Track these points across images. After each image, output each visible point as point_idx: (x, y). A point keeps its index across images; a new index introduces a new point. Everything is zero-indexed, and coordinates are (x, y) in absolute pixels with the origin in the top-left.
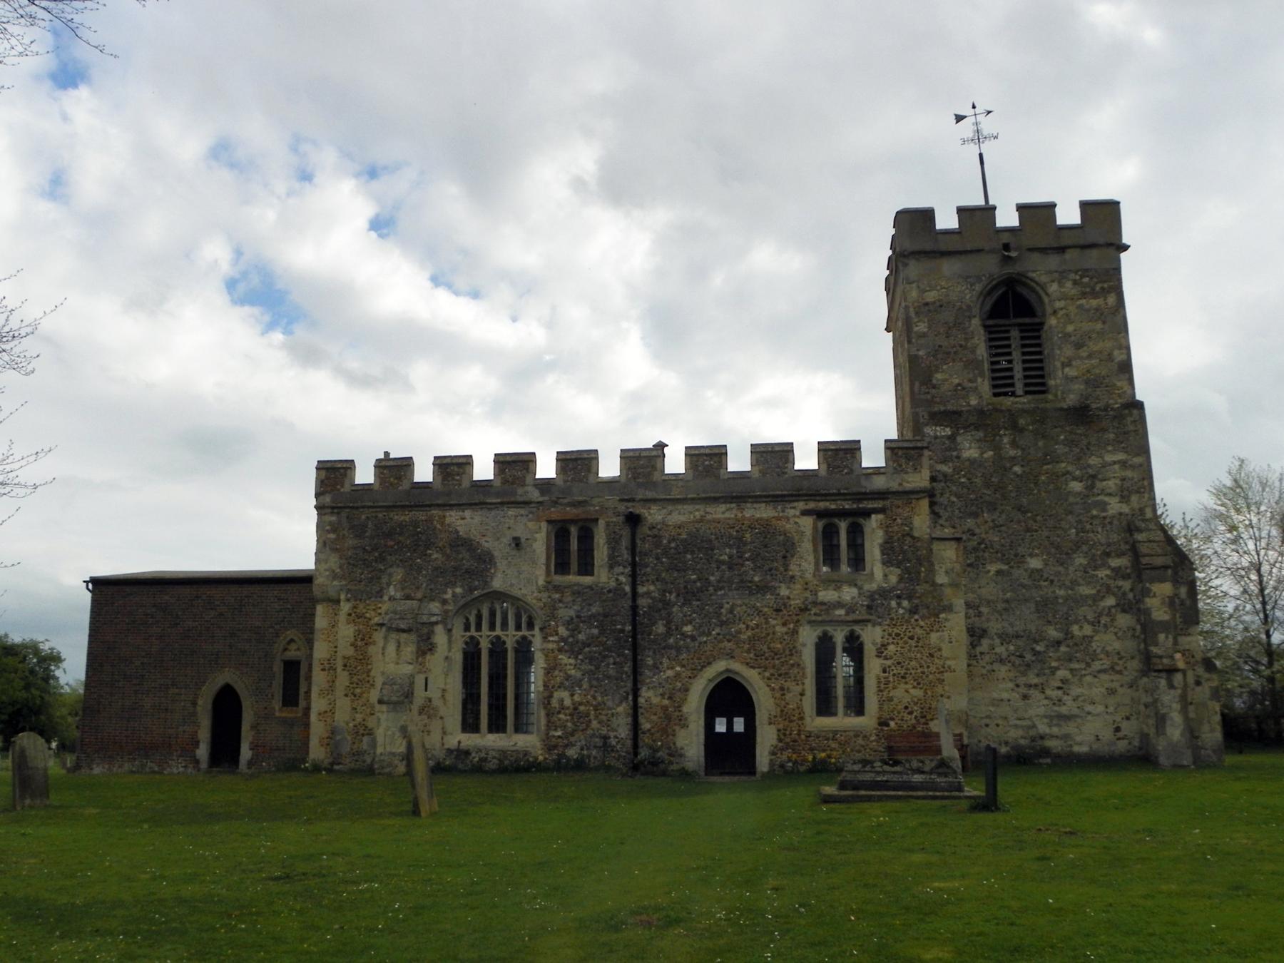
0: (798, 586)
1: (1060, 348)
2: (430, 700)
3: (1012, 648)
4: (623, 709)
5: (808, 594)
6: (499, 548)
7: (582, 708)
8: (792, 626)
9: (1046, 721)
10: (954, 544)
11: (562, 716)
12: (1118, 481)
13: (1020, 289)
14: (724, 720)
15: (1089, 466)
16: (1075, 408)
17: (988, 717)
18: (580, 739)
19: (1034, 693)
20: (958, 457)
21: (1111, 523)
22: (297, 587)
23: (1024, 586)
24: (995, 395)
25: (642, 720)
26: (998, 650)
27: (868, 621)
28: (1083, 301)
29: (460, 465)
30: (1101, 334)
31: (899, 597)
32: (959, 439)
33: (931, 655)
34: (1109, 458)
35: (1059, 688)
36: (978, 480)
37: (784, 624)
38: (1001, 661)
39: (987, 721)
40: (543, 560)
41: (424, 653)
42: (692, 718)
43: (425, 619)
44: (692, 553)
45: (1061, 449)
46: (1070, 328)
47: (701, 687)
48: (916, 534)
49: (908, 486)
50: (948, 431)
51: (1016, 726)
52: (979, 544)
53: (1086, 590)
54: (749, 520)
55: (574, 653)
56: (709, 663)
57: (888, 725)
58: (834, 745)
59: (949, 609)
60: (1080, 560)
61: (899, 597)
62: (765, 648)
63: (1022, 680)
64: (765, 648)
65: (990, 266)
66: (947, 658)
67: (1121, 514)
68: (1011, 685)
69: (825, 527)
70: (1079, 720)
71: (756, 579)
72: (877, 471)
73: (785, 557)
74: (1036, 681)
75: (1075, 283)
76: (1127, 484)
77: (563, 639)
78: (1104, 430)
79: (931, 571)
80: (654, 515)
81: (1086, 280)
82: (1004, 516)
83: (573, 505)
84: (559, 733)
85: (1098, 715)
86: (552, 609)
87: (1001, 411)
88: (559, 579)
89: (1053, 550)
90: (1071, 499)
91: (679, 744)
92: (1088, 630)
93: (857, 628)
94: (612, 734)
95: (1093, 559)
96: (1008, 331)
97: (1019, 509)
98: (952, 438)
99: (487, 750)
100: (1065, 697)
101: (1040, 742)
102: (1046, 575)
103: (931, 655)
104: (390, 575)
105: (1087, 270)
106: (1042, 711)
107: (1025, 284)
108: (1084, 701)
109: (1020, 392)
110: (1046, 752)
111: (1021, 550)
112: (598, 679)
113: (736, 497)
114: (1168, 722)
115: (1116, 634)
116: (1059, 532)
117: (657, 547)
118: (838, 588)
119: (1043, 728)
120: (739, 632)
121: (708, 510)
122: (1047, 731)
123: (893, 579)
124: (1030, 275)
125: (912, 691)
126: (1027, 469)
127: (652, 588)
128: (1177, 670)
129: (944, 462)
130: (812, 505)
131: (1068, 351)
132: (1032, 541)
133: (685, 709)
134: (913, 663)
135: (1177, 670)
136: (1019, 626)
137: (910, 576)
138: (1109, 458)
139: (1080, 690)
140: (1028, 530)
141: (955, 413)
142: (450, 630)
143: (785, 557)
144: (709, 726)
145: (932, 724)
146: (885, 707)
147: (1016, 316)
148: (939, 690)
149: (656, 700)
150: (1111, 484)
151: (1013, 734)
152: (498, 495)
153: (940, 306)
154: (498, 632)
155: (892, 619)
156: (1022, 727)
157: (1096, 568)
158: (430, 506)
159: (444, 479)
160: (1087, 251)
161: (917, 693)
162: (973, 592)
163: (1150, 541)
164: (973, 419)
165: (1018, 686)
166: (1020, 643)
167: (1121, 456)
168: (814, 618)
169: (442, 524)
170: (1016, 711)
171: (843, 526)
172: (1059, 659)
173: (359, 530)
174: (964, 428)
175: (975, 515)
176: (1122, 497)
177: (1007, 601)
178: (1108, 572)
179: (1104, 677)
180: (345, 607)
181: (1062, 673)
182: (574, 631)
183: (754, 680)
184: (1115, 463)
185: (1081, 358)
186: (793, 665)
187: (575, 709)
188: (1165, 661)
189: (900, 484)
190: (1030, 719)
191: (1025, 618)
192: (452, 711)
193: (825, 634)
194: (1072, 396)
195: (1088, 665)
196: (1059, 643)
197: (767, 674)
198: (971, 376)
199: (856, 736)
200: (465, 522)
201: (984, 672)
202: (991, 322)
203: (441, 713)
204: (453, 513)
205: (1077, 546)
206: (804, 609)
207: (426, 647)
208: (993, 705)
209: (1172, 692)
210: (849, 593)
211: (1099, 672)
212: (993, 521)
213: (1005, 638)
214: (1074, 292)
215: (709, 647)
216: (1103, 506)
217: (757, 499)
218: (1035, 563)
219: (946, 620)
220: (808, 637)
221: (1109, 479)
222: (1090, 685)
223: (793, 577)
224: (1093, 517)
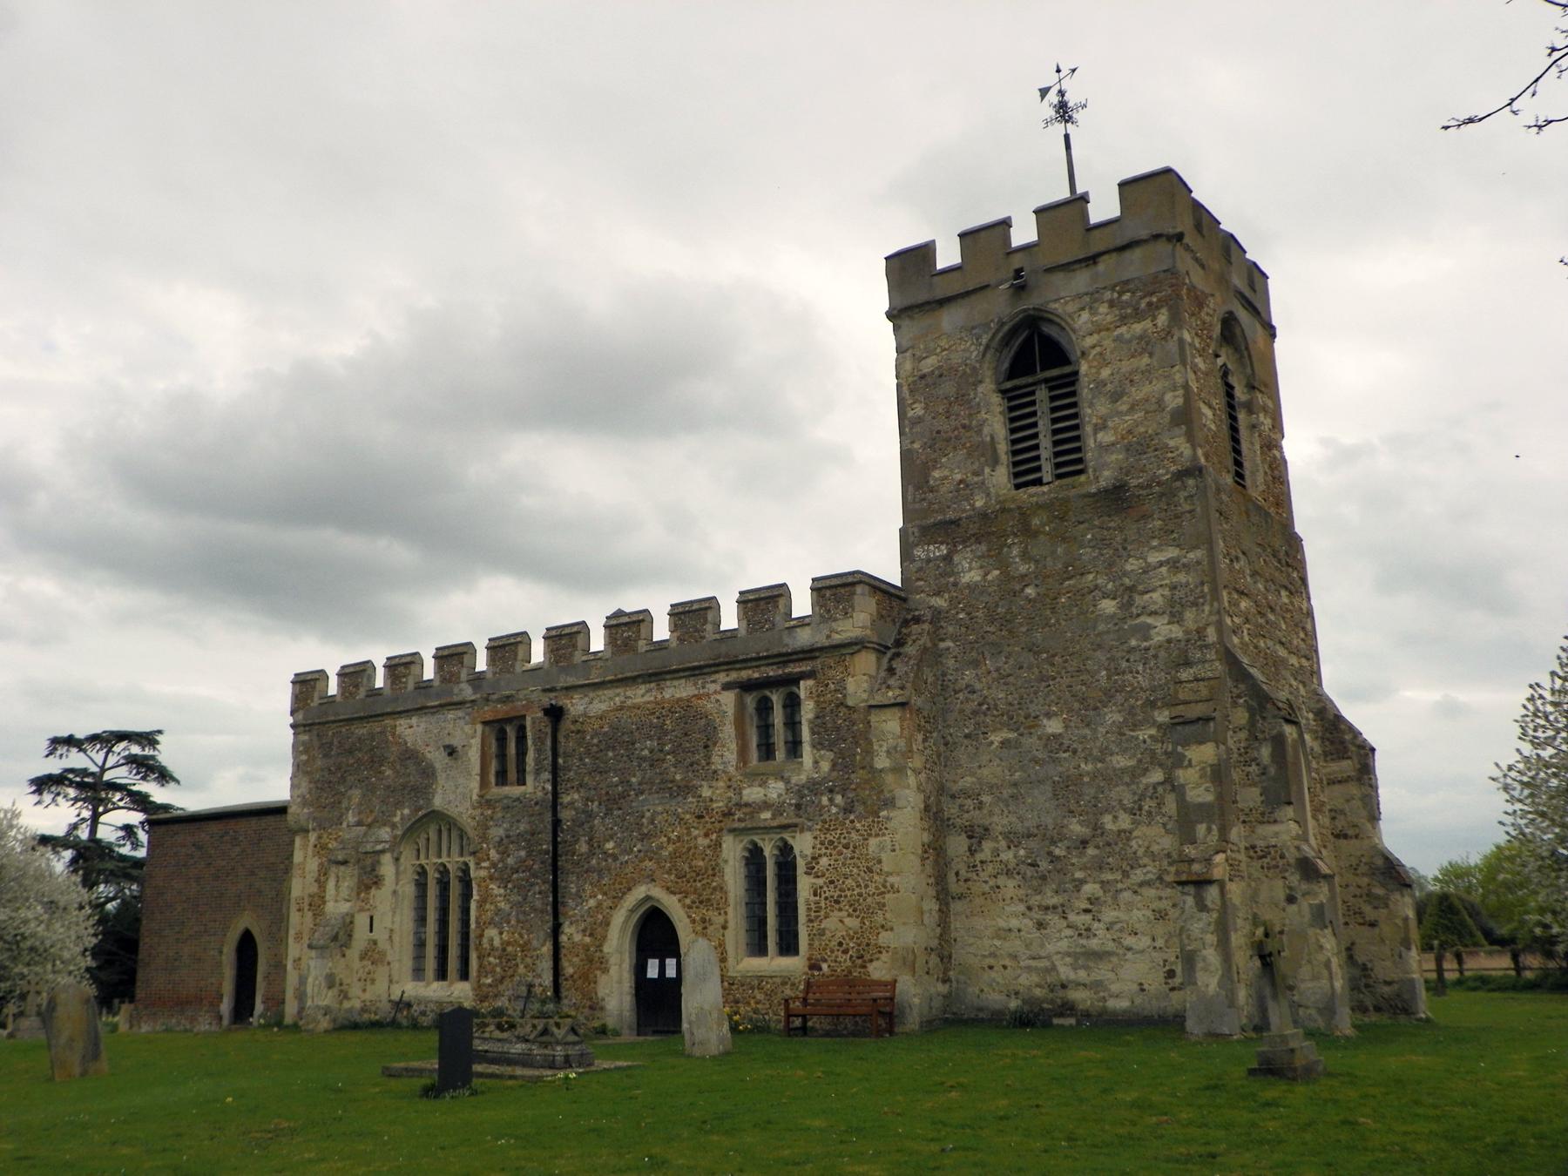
0: (721, 784)
1: (1091, 405)
2: (375, 943)
3: (1022, 852)
4: (547, 949)
5: (731, 794)
6: (437, 757)
7: (510, 949)
8: (714, 837)
9: (1068, 960)
10: (897, 712)
11: (491, 959)
12: (1167, 592)
13: (1048, 329)
14: (657, 961)
15: (1125, 574)
16: (1106, 491)
17: (993, 955)
18: (507, 988)
19: (1053, 919)
20: (955, 584)
21: (1155, 657)
22: (271, 819)
23: (1035, 761)
24: (1018, 487)
25: (565, 963)
26: (1003, 856)
27: (796, 825)
28: (1123, 329)
29: (407, 665)
30: (1147, 373)
31: (831, 791)
32: (956, 558)
33: (870, 870)
34: (1154, 558)
35: (1087, 911)
36: (979, 614)
37: (706, 835)
38: (1008, 873)
39: (991, 961)
40: (477, 769)
41: (368, 888)
42: (613, 960)
43: (369, 848)
44: (614, 748)
45: (1086, 553)
46: (1105, 373)
47: (622, 919)
48: (850, 703)
49: (837, 638)
50: (944, 550)
51: (1029, 969)
52: (980, 704)
53: (1121, 761)
54: (669, 701)
55: (504, 882)
56: (630, 889)
57: (820, 969)
58: (760, 996)
59: (890, 803)
60: (1113, 716)
61: (831, 791)
62: (686, 868)
63: (1035, 900)
64: (686, 868)
65: (999, 307)
66: (889, 874)
67: (1169, 641)
68: (1022, 908)
69: (759, 702)
70: (1115, 959)
71: (678, 777)
72: (803, 622)
73: (706, 747)
74: (1055, 900)
75: (1112, 304)
76: (1179, 594)
77: (494, 865)
78: (1145, 517)
79: (869, 752)
80: (576, 706)
81: (1126, 297)
82: (1011, 661)
83: (500, 701)
84: (489, 981)
85: (1142, 951)
86: (484, 826)
87: (1010, 510)
88: (496, 791)
89: (1076, 705)
90: (1101, 627)
91: (600, 995)
92: (1125, 821)
93: (787, 836)
94: (537, 981)
95: (1131, 712)
96: (1033, 393)
97: (1032, 649)
98: (948, 558)
99: (427, 1001)
100: (1096, 925)
101: (1061, 993)
102: (1066, 742)
103: (870, 870)
104: (350, 798)
105: (1127, 282)
106: (1063, 945)
107: (1050, 321)
108: (1121, 930)
109: (1047, 477)
110: (1067, 1008)
111: (1034, 709)
112: (524, 913)
113: (655, 674)
114: (1200, 965)
115: (1164, 825)
116: (1084, 677)
117: (580, 745)
118: (763, 784)
119: (1065, 972)
120: (661, 847)
121: (629, 694)
122: (1072, 976)
123: (825, 766)
124: (1053, 306)
125: (847, 920)
126: (1042, 590)
127: (576, 796)
128: (1210, 882)
129: (938, 593)
130: (734, 676)
131: (1102, 407)
132: (1047, 695)
133: (606, 949)
134: (849, 882)
135: (1210, 882)
136: (1031, 821)
137: (843, 764)
138: (1154, 558)
139: (1115, 913)
140: (1042, 679)
141: (952, 522)
142: (397, 859)
143: (706, 747)
144: (640, 969)
145: (871, 967)
146: (816, 943)
147: (1042, 370)
148: (879, 919)
149: (577, 938)
150: (1157, 598)
151: (1025, 980)
152: (438, 696)
153: (940, 375)
154: (444, 859)
155: (825, 822)
156: (1036, 969)
157: (1135, 727)
158: (382, 715)
159: (393, 683)
160: (1127, 254)
161: (852, 923)
162: (973, 774)
163: (1197, 680)
164: (973, 529)
165: (1029, 908)
166: (1033, 844)
167: (1172, 553)
168: (736, 825)
169: (393, 735)
170: (1027, 946)
171: (776, 698)
172: (1084, 868)
173: (326, 749)
174: (964, 542)
175: (975, 664)
176: (1172, 615)
177: (1015, 785)
178: (1153, 731)
179: (1151, 892)
180: (313, 837)
181: (1090, 888)
182: (504, 853)
183: (674, 907)
184: (1161, 564)
185: (1119, 414)
186: (715, 889)
187: (504, 950)
188: (1196, 867)
189: (828, 637)
190: (1048, 957)
191: (1040, 808)
192: (400, 955)
193: (755, 844)
194: (1106, 473)
195: (1126, 874)
196: (1084, 843)
197: (688, 901)
198: (975, 466)
199: (784, 984)
200: (412, 730)
201: (987, 888)
202: (1009, 385)
203: (389, 958)
204: (402, 721)
205: (1109, 695)
206: (728, 814)
207: (370, 880)
208: (999, 937)
209: (1204, 915)
210: (775, 789)
211: (1141, 885)
212: (997, 670)
213: (1013, 838)
214: (1109, 318)
215: (630, 869)
216: (1145, 632)
217: (675, 674)
218: (1054, 726)
219: (889, 819)
220: (733, 852)
221: (1153, 590)
222: (1130, 906)
223: (715, 772)
224: (1131, 650)
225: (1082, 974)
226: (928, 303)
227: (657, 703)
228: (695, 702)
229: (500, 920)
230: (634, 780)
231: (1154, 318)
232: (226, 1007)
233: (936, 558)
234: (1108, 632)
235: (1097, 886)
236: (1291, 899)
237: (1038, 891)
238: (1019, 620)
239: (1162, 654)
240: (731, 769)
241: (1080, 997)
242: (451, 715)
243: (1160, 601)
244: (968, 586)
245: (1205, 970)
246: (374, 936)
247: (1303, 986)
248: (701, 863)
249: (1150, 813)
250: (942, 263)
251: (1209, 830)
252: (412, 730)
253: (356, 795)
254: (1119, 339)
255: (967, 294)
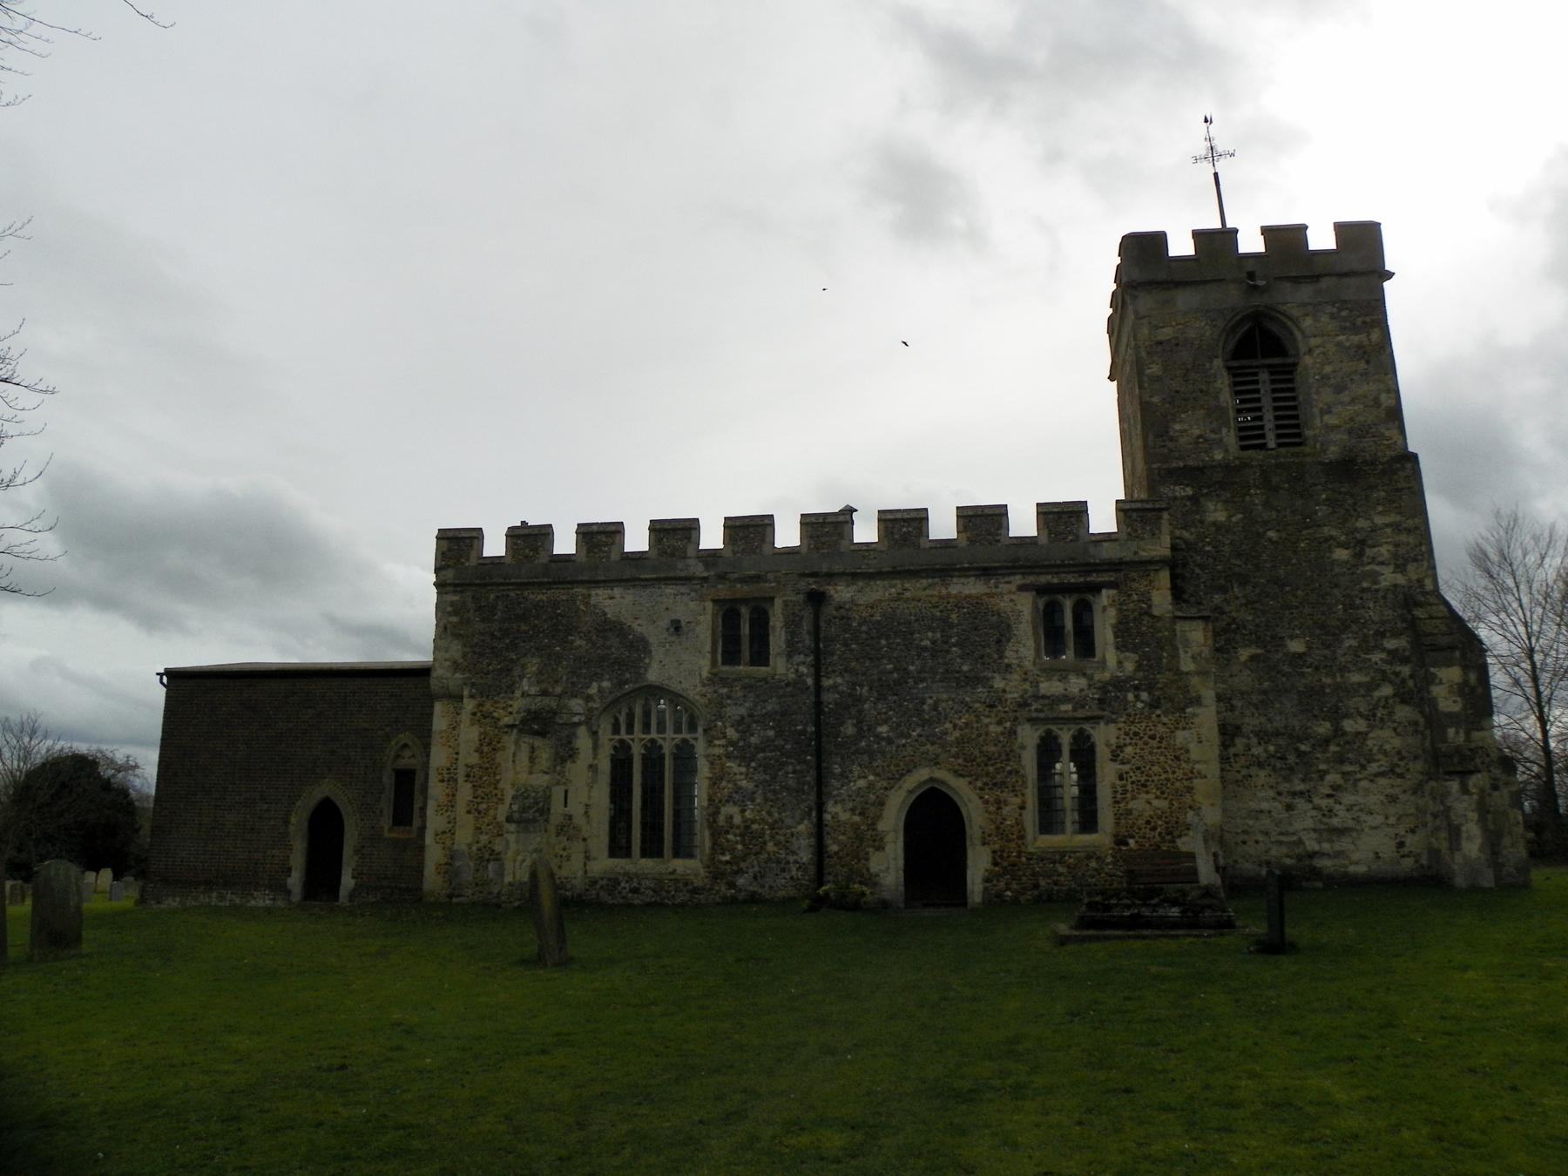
0: (1016, 676)
1: (1318, 393)
2: (570, 817)
5: (1027, 686)
6: (654, 634)
7: (755, 826)
8: (1008, 725)
11: (730, 837)
15: (1356, 530)
17: (1245, 832)
19: (1301, 804)
20: (1202, 522)
21: (1384, 597)
24: (1244, 448)
25: (828, 841)
27: (1101, 718)
28: (1341, 338)
31: (1137, 688)
35: (1329, 796)
37: (999, 723)
38: (1260, 765)
40: (708, 647)
41: (563, 761)
42: (888, 838)
44: (888, 638)
46: (1328, 369)
49: (1144, 555)
51: (1280, 843)
53: (1356, 678)
54: (956, 596)
56: (909, 771)
57: (1127, 844)
58: (1061, 869)
60: (1350, 642)
61: (1137, 688)
62: (976, 752)
63: (1284, 787)
64: (976, 752)
65: (1233, 297)
67: (1395, 586)
68: (1272, 793)
69: (1047, 605)
72: (1107, 537)
73: (999, 642)
74: (1300, 787)
75: (1332, 316)
76: (1402, 551)
78: (1372, 488)
79: (1175, 656)
80: (842, 593)
81: (1344, 313)
92: (1361, 725)
93: (1086, 726)
96: (1256, 374)
98: (1194, 499)
103: (1177, 758)
104: (524, 667)
106: (1309, 823)
109: (1272, 444)
110: (1316, 873)
112: (775, 791)
113: (942, 570)
114: (1464, 835)
115: (1395, 729)
119: (1311, 845)
120: (945, 733)
121: (907, 586)
122: (1317, 848)
123: (1129, 667)
126: (1284, 535)
127: (839, 680)
130: (1030, 579)
131: (1326, 396)
133: (881, 826)
134: (1156, 768)
136: (1279, 723)
138: (1379, 520)
143: (999, 642)
145: (1179, 842)
147: (1264, 357)
150: (1384, 551)
154: (654, 735)
157: (1369, 651)
159: (589, 551)
160: (1346, 280)
165: (1279, 794)
166: (1281, 742)
167: (1393, 518)
168: (1034, 715)
169: (587, 604)
171: (1068, 604)
172: (1327, 761)
176: (1397, 566)
178: (1384, 656)
179: (1382, 781)
180: (469, 705)
181: (1333, 777)
184: (1387, 525)
186: (1010, 772)
187: (747, 827)
195: (1363, 767)
198: (1214, 425)
199: (1089, 857)
200: (615, 603)
201: (1239, 777)
202: (1235, 364)
203: (584, 834)
204: (600, 592)
206: (1023, 704)
207: (566, 753)
210: (1076, 684)
212: (1245, 597)
214: (1330, 327)
216: (1375, 577)
217: (964, 572)
218: (1296, 646)
219: (1195, 715)
224: (1363, 590)
225: (1326, 846)
226: (1167, 282)
227: (941, 598)
228: (986, 599)
229: (740, 797)
230: (911, 668)
231: (1369, 334)
232: (295, 881)
233: (1182, 498)
234: (1343, 574)
235: (1338, 776)
236: (1495, 788)
237: (1287, 779)
238: (1264, 557)
239: (1390, 596)
240: (1028, 664)
241: (1325, 864)
242: (669, 590)
243: (1387, 555)
244: (1214, 524)
245: (1468, 838)
246: (570, 810)
247: (1505, 852)
248: (993, 749)
249: (1382, 720)
250: (1174, 251)
251: (1457, 733)
252: (615, 603)
253: (533, 664)
254: (1339, 344)
255: (1206, 282)
